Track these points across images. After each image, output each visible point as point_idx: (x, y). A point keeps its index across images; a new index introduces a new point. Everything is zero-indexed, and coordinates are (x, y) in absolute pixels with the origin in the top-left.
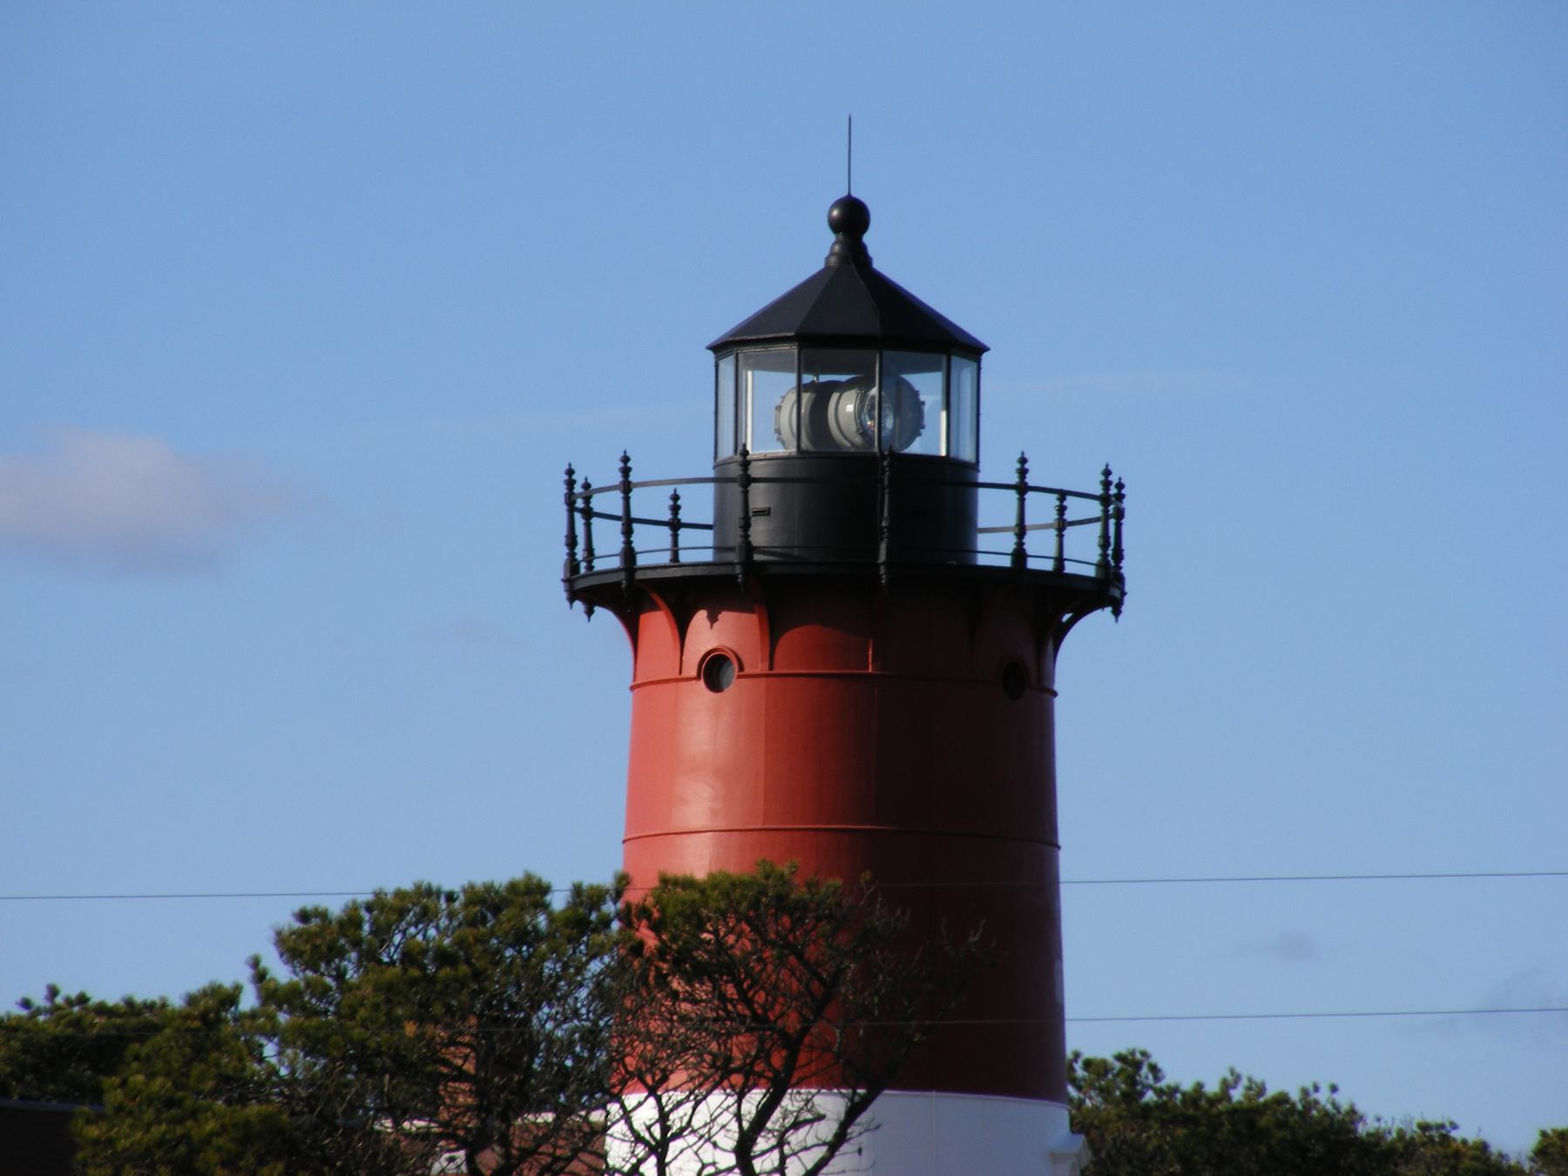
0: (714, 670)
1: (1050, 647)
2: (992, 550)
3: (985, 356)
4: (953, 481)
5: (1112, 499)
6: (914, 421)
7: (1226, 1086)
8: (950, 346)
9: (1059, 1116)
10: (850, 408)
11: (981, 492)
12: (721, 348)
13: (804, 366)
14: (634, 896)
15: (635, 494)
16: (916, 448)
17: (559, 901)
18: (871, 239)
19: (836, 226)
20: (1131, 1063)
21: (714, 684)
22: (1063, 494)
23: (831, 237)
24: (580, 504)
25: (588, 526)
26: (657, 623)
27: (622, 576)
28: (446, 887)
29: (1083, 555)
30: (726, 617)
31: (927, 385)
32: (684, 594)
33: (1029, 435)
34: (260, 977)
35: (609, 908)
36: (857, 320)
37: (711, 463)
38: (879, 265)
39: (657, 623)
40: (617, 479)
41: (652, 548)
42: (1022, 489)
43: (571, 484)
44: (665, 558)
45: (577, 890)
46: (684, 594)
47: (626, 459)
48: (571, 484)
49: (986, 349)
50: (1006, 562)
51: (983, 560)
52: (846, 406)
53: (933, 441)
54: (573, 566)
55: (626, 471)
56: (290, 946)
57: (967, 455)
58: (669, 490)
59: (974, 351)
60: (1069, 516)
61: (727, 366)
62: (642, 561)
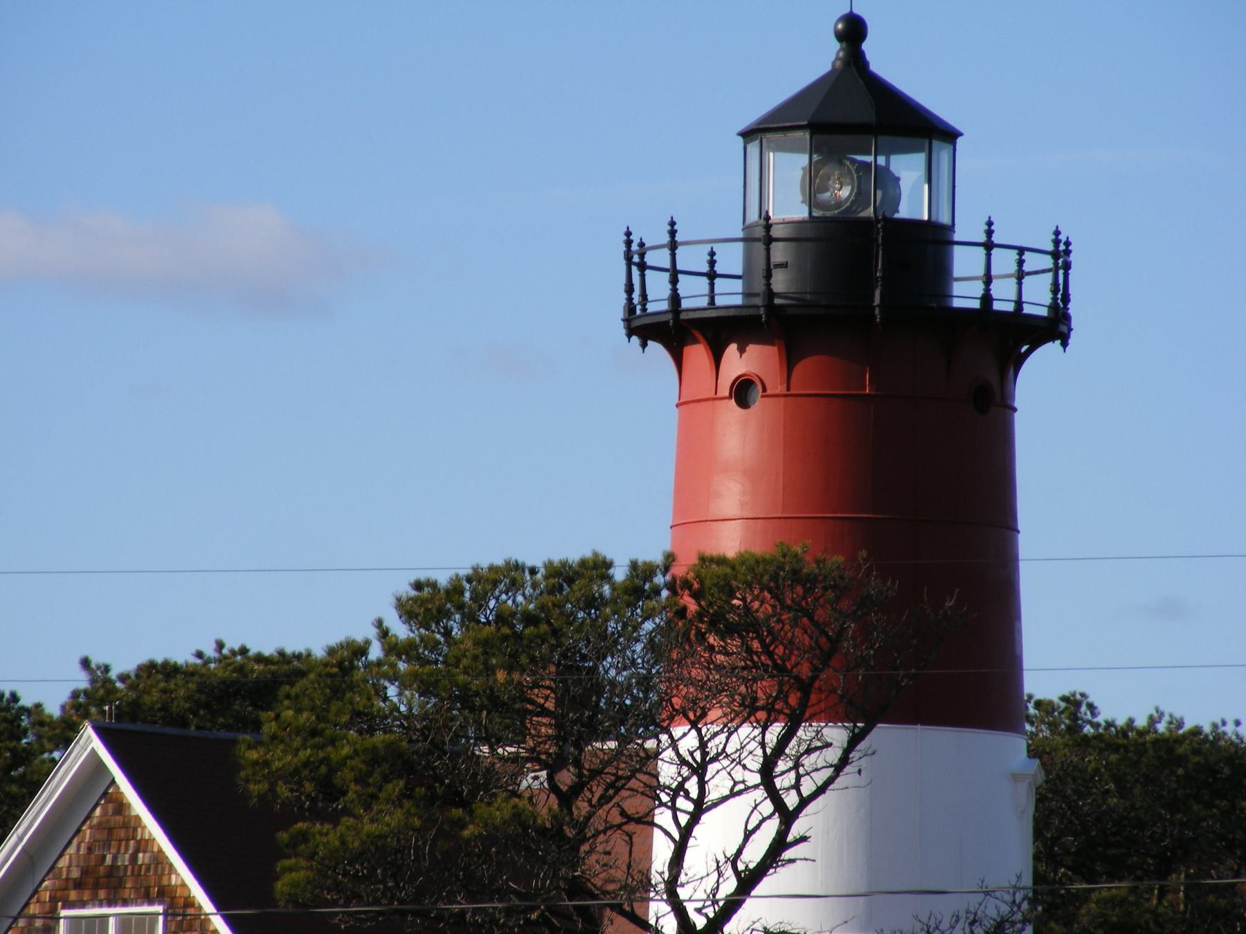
0: (742, 391)
1: (1012, 372)
2: (965, 295)
3: (959, 140)
4: (933, 240)
5: (1061, 254)
7: (1153, 721)
8: (923, 130)
11: (956, 248)
12: (748, 135)
17: (620, 574)
19: (840, 36)
21: (743, 402)
22: (1021, 251)
24: (636, 259)
25: (643, 277)
26: (697, 354)
27: (669, 316)
28: (529, 563)
29: (1038, 298)
30: (752, 349)
32: (719, 331)
33: (992, 204)
34: (384, 634)
35: (659, 580)
36: (857, 112)
37: (741, 226)
39: (697, 354)
40: (666, 239)
41: (694, 294)
42: (989, 246)
45: (634, 565)
46: (719, 331)
47: (672, 224)
48: (629, 243)
49: (960, 134)
50: (976, 304)
51: (957, 303)
53: (913, 204)
54: (630, 308)
55: (673, 233)
56: (407, 610)
57: (945, 219)
58: (707, 248)
59: (950, 135)
60: (1026, 268)
61: (754, 149)
62: (685, 304)
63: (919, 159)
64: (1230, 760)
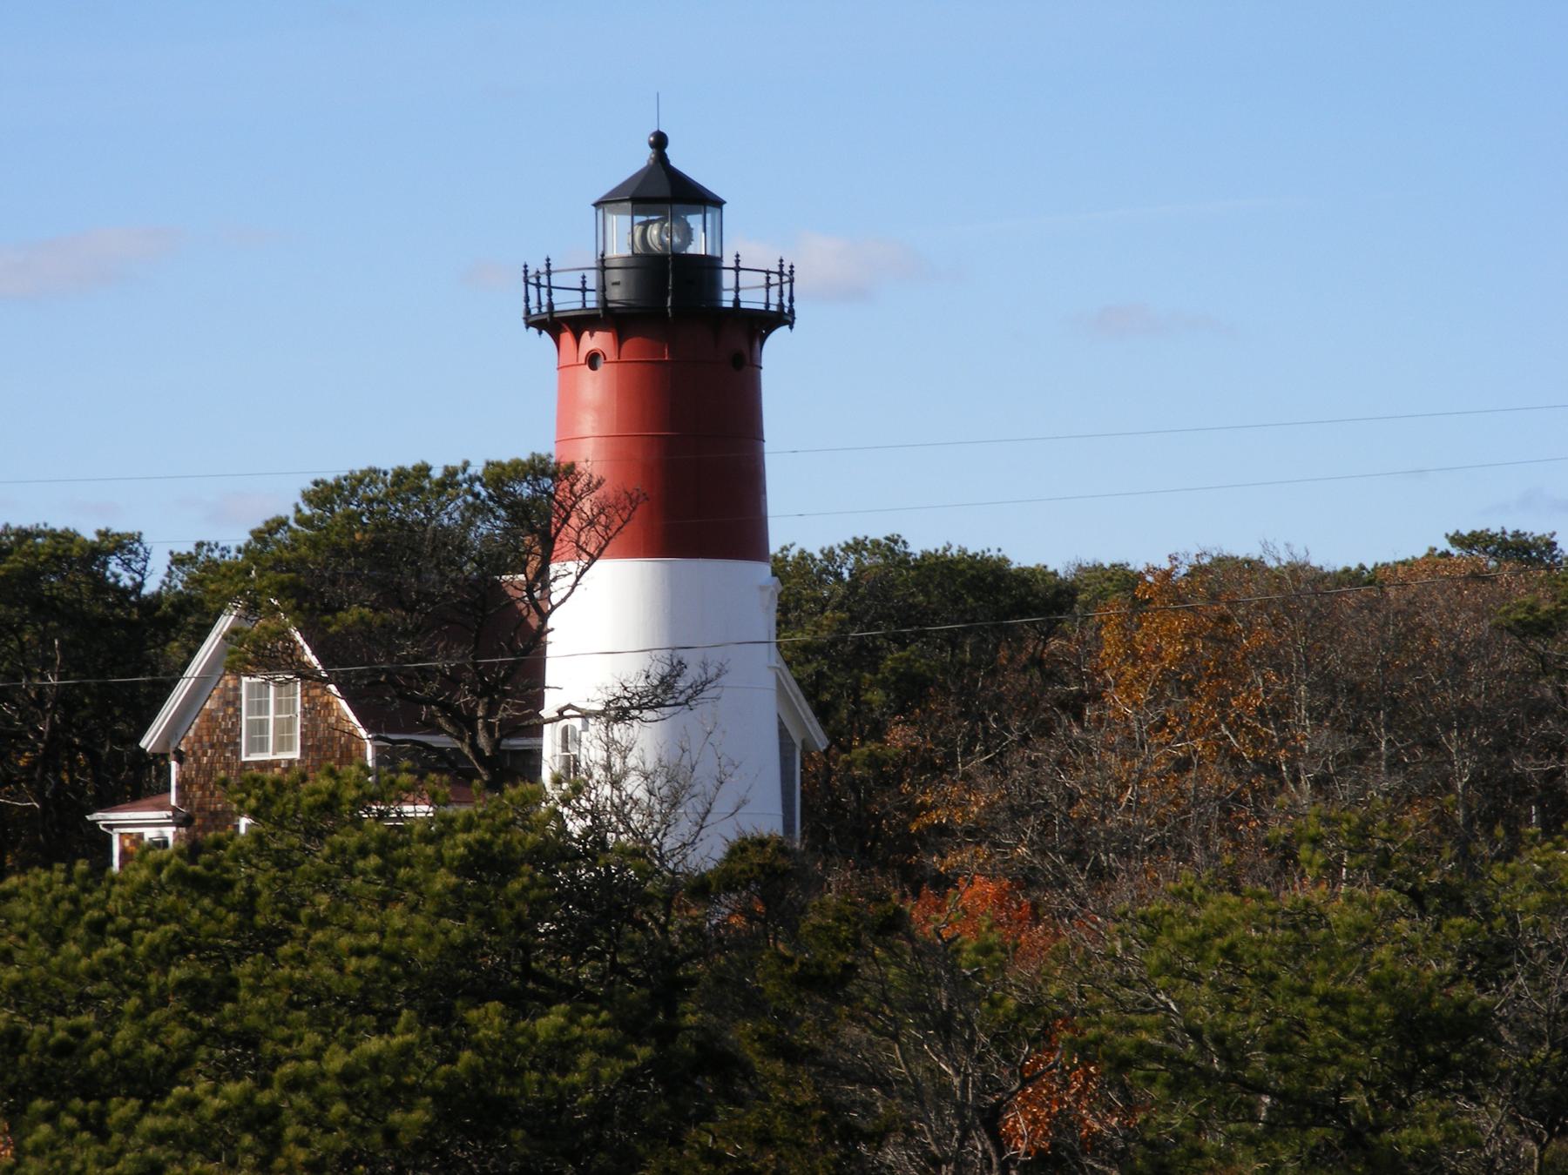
0: (593, 360)
1: (758, 345)
2: (727, 300)
4: (709, 266)
6: (688, 235)
7: (945, 550)
8: (700, 199)
9: (764, 570)
10: (655, 232)
12: (597, 205)
13: (634, 213)
14: (471, 471)
15: (553, 276)
16: (691, 250)
17: (437, 474)
18: (669, 151)
19: (652, 145)
20: (893, 540)
21: (593, 367)
22: (768, 272)
23: (650, 150)
24: (533, 280)
25: (550, 294)
26: (567, 337)
28: (383, 468)
30: (597, 334)
31: (695, 221)
32: (579, 324)
33: (745, 248)
34: (298, 510)
35: (460, 477)
36: (665, 190)
38: (672, 163)
39: (567, 337)
42: (737, 269)
43: (526, 272)
44: (579, 306)
45: (446, 468)
46: (579, 324)
48: (526, 272)
52: (654, 231)
53: (698, 247)
54: (528, 311)
56: (308, 498)
58: (580, 273)
59: (718, 203)
61: (600, 213)
62: (557, 308)
63: (699, 217)
64: (993, 572)
